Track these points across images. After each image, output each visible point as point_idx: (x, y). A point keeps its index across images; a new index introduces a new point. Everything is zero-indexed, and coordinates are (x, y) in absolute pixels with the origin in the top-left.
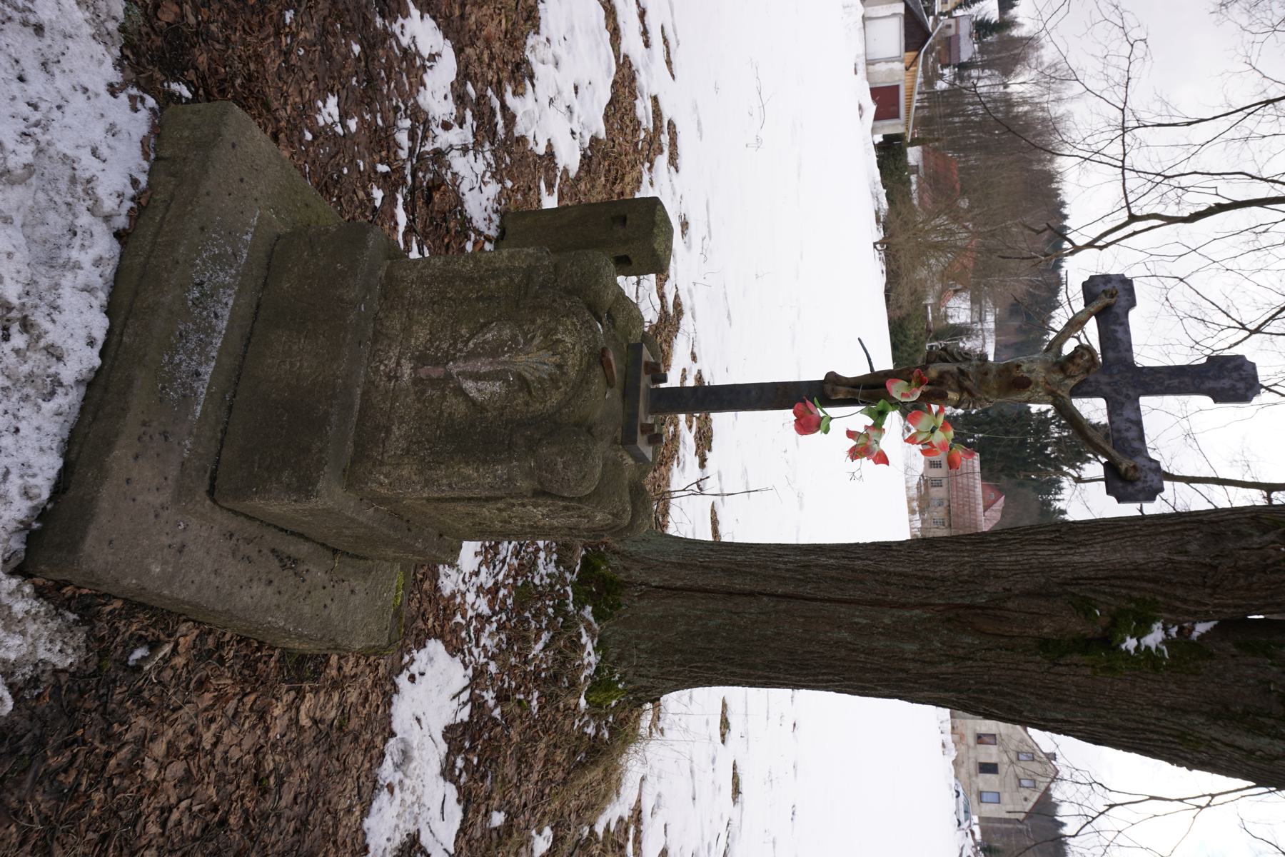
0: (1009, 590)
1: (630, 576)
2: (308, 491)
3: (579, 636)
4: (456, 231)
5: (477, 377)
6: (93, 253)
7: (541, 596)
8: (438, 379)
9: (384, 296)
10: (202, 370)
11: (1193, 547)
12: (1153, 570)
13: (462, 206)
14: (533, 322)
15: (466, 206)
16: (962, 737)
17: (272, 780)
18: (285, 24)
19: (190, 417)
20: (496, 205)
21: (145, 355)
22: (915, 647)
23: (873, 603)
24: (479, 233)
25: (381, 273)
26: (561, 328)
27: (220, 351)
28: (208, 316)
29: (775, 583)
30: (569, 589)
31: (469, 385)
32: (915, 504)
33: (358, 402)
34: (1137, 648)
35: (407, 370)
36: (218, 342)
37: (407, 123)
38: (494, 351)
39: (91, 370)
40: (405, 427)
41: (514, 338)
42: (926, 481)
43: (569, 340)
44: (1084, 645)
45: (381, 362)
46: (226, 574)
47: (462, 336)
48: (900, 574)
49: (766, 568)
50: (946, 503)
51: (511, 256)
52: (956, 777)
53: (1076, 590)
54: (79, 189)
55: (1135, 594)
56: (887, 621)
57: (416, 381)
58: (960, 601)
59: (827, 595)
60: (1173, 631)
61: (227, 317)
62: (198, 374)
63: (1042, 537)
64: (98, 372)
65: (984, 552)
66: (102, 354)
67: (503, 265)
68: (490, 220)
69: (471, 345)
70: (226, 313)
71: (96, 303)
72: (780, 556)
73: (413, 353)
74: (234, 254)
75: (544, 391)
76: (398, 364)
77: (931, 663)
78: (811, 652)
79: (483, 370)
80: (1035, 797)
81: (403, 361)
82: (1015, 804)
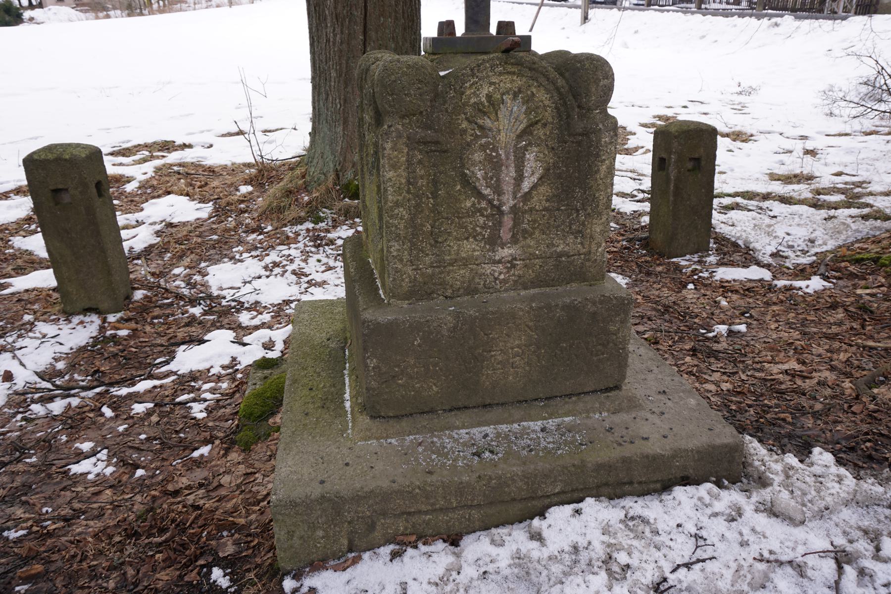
2: (628, 304)
4: (115, 344)
5: (519, 178)
6: (493, 551)
8: (514, 220)
9: (429, 295)
10: (538, 428)
13: (85, 347)
14: (464, 131)
15: (83, 344)
17: (646, 336)
18: (29, 534)
19: (579, 422)
20: (61, 322)
21: (574, 465)
24: (102, 329)
25: (405, 304)
26: (472, 101)
27: (513, 422)
28: (492, 440)
29: (353, 42)
31: (526, 185)
32: (101, 15)
33: (532, 291)
35: (505, 252)
36: (504, 428)
37: (37, 408)
38: (495, 165)
39: (600, 501)
41: (483, 148)
42: (77, 5)
43: (486, 90)
45: (496, 279)
46: (644, 366)
47: (474, 205)
49: (341, 51)
51: (394, 167)
57: (514, 240)
61: (479, 429)
64: (597, 496)
66: (581, 500)
67: (405, 174)
68: (82, 322)
69: (487, 191)
70: (476, 431)
72: (328, 41)
73: (489, 250)
74: (420, 444)
75: (537, 108)
76: (499, 262)
78: (403, 13)
79: (513, 174)
81: (497, 258)
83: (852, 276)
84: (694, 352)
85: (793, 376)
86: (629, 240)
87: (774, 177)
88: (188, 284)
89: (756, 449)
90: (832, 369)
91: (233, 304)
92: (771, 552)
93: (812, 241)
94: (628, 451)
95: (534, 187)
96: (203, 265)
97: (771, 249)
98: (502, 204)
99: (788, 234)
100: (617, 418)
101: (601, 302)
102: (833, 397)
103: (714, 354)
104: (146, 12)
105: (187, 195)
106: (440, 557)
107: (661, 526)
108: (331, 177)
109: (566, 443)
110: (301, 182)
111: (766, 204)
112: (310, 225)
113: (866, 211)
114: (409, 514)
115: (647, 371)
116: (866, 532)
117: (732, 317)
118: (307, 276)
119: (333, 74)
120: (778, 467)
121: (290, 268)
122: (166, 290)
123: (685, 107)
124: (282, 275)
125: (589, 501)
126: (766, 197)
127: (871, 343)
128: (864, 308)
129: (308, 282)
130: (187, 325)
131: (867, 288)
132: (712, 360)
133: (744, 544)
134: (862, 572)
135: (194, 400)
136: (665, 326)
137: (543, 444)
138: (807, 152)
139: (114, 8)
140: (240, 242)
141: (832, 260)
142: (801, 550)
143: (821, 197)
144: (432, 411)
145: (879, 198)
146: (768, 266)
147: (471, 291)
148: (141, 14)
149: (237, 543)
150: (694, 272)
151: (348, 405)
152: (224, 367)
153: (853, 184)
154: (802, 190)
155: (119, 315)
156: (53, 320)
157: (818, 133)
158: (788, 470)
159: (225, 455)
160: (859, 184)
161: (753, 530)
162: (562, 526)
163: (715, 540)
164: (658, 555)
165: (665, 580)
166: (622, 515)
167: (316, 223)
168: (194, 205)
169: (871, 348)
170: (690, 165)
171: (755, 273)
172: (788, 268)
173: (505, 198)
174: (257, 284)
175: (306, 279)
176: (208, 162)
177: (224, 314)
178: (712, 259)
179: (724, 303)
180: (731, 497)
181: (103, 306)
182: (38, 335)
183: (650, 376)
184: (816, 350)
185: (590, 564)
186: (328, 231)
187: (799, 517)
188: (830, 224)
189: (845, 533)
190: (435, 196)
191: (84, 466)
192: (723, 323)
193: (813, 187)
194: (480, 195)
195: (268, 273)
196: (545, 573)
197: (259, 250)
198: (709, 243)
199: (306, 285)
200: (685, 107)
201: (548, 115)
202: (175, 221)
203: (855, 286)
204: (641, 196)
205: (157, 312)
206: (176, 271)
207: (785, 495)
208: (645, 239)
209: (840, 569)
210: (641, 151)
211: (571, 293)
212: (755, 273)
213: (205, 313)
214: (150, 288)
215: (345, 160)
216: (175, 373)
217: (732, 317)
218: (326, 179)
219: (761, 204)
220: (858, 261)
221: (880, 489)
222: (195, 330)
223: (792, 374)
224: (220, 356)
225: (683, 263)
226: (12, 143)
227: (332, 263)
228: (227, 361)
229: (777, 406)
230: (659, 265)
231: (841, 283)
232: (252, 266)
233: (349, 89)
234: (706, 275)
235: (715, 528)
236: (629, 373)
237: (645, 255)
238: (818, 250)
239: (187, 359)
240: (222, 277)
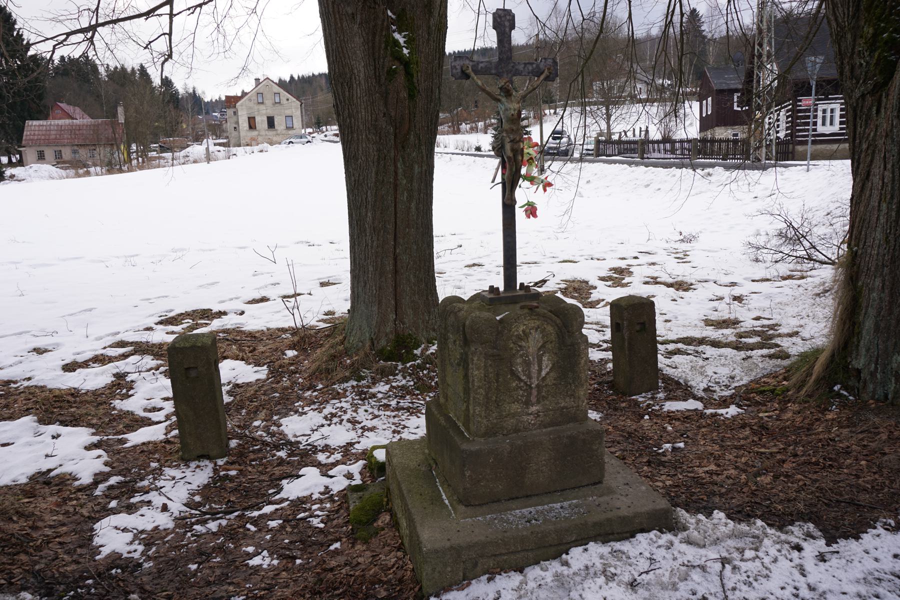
0: (385, 114)
1: (391, 332)
3: (432, 353)
5: (540, 370)
7: (419, 379)
9: (495, 434)
11: (350, 10)
12: (367, 34)
14: (512, 349)
16: (253, 139)
22: (416, 167)
23: (395, 189)
24: (215, 471)
25: (482, 440)
30: (408, 365)
31: (543, 373)
32: (81, 171)
33: (549, 429)
34: (407, 48)
35: (534, 409)
36: (540, 508)
38: (527, 364)
40: (560, 401)
41: (521, 356)
42: (58, 163)
43: (522, 328)
44: (408, 74)
48: (377, 174)
49: (377, 253)
50: (76, 148)
51: (478, 369)
52: (280, 143)
53: (383, 78)
54: (522, 592)
55: (383, 46)
56: (405, 182)
57: (538, 402)
58: (393, 142)
59: (393, 216)
60: (394, 28)
62: (562, 507)
63: (347, 93)
65: (358, 127)
66: (587, 544)
69: (524, 378)
71: (568, 557)
72: (367, 245)
76: (531, 414)
77: (422, 158)
79: (537, 368)
80: (285, 94)
82: (293, 107)
83: (758, 403)
84: (649, 463)
85: (711, 474)
86: (599, 384)
87: (708, 323)
88: (268, 434)
89: (682, 513)
90: (736, 468)
91: (309, 447)
92: (688, 561)
93: (733, 378)
94: (609, 515)
95: (548, 374)
96: (275, 418)
97: (703, 386)
98: (532, 383)
99: (715, 373)
100: (602, 499)
101: (587, 433)
102: (733, 484)
103: (662, 464)
104: (125, 168)
105: (242, 360)
106: (516, 579)
107: (631, 554)
108: (368, 344)
109: (575, 513)
110: (341, 348)
111: (700, 348)
112: (355, 383)
113: (772, 351)
114: (495, 555)
115: (616, 473)
116: (738, 549)
117: (674, 438)
118: (360, 423)
119: (371, 269)
120: (693, 521)
121: (345, 417)
122: (253, 438)
123: (636, 258)
124: (341, 424)
125: (592, 543)
126: (702, 341)
127: (763, 450)
128: (763, 427)
129: (362, 428)
130: (279, 465)
131: (766, 412)
132: (661, 468)
133: (675, 559)
134: (734, 568)
135: (311, 517)
136: (630, 447)
137: (563, 514)
138: (736, 298)
139: (95, 165)
140: (299, 398)
141: (744, 393)
142: (704, 559)
143: (743, 340)
144: (499, 501)
145: (785, 339)
146: (700, 399)
147: (517, 431)
148: (121, 171)
149: (386, 590)
150: (649, 406)
151: (447, 502)
152: (321, 493)
153: (768, 326)
154: (728, 334)
155: (225, 459)
156: (175, 466)
157: (745, 279)
158: (699, 521)
159: (353, 547)
160: (772, 327)
161: (680, 552)
162: (577, 557)
163: (660, 559)
164: (630, 568)
165: (635, 580)
166: (610, 549)
167: (359, 381)
168: (250, 368)
169: (762, 453)
170: (638, 328)
171: (692, 405)
172: (715, 400)
173: (533, 380)
174: (323, 430)
175: (360, 426)
176: (247, 328)
177: (304, 456)
178: (661, 395)
179: (670, 428)
180: (667, 537)
181: (213, 453)
182: (168, 477)
183: (619, 476)
184: (729, 456)
185: (595, 574)
186: (369, 387)
187: (702, 543)
188: (746, 364)
189: (727, 551)
190: (497, 381)
191: (256, 561)
192: (668, 442)
193: (738, 331)
194: (520, 380)
195: (328, 422)
196: (572, 582)
197: (319, 404)
198: (658, 383)
199: (361, 431)
200: (636, 258)
201: (553, 337)
202: (240, 382)
203: (759, 411)
204: (605, 345)
205: (252, 456)
206: (256, 423)
207: (696, 533)
208: (611, 382)
209: (724, 567)
210: (602, 304)
211: (570, 429)
212: (692, 405)
213: (289, 455)
214: (240, 438)
215: (379, 331)
216: (287, 500)
217: (674, 438)
218: (364, 346)
219: (697, 348)
220: (762, 392)
221: (748, 528)
222: (287, 469)
223: (710, 473)
224: (316, 486)
225: (641, 400)
226: (72, 315)
227: (376, 412)
228: (322, 489)
229: (699, 492)
230: (623, 402)
231: (750, 409)
232: (313, 418)
233: (383, 279)
234: (657, 408)
235: (659, 554)
236: (606, 475)
237: (612, 395)
238: (736, 384)
239: (292, 489)
240: (294, 426)
